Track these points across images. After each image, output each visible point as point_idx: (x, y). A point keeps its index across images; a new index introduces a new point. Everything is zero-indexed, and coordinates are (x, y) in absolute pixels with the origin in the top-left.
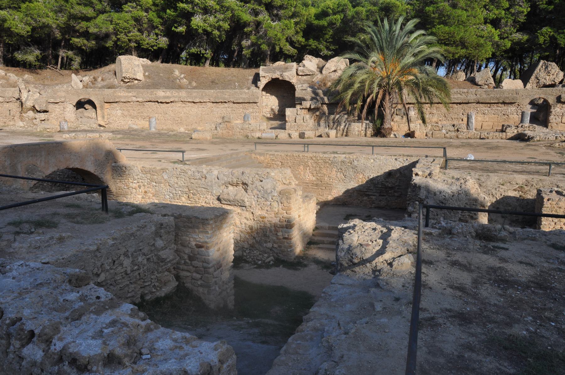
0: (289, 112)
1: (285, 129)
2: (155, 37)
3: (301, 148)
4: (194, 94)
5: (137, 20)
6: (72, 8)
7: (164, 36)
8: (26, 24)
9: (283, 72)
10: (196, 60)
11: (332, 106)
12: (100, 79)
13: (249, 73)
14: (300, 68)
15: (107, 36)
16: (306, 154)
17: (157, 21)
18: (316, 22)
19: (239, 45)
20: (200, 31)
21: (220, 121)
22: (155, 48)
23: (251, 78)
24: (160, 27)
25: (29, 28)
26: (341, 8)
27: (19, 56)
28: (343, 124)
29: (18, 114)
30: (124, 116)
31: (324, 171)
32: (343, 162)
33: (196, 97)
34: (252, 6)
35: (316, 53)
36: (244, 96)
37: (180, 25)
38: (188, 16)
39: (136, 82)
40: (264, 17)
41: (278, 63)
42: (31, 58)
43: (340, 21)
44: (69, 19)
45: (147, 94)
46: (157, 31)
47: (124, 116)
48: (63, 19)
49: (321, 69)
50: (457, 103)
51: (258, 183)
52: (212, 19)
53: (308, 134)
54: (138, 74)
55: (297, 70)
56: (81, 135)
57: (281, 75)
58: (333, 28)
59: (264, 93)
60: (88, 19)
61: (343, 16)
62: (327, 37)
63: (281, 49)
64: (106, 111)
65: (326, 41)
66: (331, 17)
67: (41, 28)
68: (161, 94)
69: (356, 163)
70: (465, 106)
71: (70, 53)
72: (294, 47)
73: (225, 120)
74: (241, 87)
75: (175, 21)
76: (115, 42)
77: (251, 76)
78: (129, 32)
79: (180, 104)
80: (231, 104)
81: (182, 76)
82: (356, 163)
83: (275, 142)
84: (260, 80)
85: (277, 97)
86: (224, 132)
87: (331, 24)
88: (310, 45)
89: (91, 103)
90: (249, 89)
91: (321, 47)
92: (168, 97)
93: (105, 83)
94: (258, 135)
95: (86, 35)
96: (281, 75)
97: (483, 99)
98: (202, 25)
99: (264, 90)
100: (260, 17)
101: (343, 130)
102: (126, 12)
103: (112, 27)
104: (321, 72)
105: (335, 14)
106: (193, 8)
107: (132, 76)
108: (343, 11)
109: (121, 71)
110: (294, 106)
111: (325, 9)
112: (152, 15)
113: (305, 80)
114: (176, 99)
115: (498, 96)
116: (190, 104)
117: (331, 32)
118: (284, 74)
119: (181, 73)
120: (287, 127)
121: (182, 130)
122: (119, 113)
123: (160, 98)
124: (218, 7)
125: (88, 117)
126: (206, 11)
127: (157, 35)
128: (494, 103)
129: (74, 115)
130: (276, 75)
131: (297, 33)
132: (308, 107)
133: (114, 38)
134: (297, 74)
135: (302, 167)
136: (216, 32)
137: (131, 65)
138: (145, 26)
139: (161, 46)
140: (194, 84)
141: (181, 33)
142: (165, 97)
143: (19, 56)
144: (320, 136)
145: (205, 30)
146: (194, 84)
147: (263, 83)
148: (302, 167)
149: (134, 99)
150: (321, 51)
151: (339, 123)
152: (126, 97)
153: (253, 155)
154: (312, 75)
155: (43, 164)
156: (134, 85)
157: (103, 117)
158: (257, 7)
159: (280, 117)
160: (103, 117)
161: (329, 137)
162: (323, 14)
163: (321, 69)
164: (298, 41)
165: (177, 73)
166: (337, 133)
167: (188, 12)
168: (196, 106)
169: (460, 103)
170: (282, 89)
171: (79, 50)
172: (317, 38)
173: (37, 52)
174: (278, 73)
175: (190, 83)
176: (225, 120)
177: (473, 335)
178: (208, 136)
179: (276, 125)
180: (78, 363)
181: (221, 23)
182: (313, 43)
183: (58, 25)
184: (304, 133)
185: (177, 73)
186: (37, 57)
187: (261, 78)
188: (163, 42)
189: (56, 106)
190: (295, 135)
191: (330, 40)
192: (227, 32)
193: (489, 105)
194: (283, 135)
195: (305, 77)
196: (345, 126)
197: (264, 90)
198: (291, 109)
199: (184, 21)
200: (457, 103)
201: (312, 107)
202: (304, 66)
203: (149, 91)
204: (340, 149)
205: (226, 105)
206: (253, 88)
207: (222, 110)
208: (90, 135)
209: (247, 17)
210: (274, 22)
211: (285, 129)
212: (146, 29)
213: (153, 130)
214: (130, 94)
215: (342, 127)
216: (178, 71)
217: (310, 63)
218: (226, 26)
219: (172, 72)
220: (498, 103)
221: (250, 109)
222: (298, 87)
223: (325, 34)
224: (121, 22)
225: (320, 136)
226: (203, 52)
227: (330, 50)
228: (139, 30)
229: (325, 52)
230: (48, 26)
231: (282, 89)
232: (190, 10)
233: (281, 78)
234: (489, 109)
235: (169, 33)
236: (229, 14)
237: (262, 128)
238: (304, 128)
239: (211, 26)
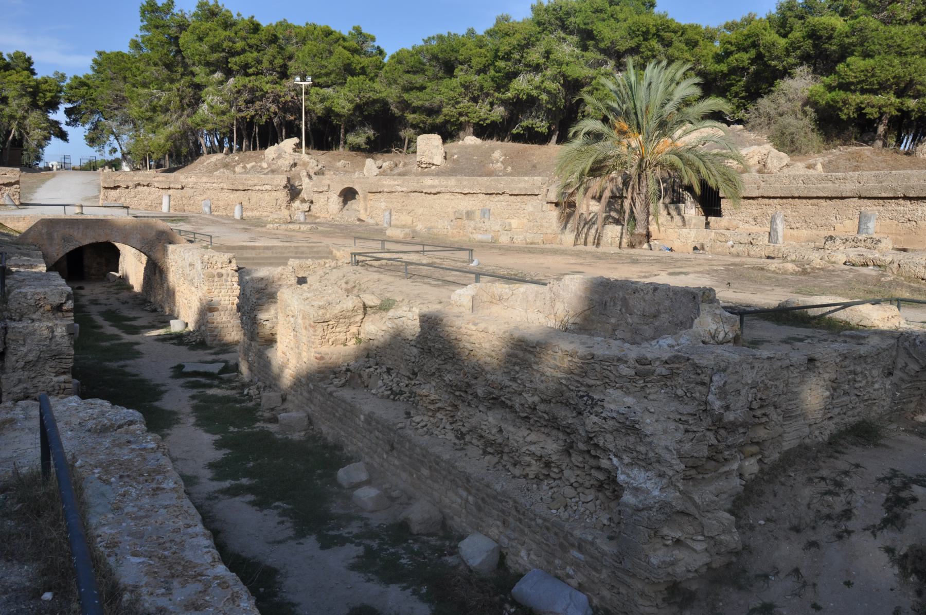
4: (465, 183)
5: (466, 86)
29: (284, 204)
33: (464, 187)
50: (826, 198)
54: (436, 158)
67: (366, 104)
70: (838, 201)
78: (458, 103)
79: (448, 196)
80: (507, 196)
92: (433, 187)
97: (867, 190)
114: (443, 189)
115: (894, 185)
116: (460, 196)
128: (891, 198)
139: (493, 119)
149: (399, 189)
155: (80, 235)
157: (366, 210)
169: (831, 198)
173: (371, 133)
177: (233, 388)
180: (415, 529)
186: (368, 138)
189: (321, 195)
191: (744, 94)
193: (881, 202)
200: (826, 198)
205: (501, 197)
214: (396, 183)
220: (897, 198)
230: (385, 103)
234: (881, 208)
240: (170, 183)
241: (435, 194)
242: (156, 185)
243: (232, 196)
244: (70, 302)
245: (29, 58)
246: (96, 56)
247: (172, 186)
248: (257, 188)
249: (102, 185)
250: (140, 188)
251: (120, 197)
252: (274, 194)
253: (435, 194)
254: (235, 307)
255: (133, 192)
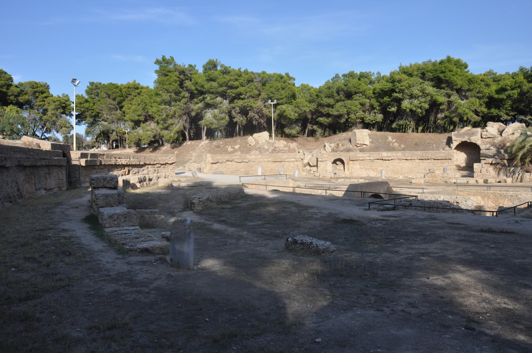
0: (476, 166)
1: (473, 177)
2: (374, 115)
3: (485, 188)
5: (362, 105)
6: (322, 100)
7: (380, 113)
8: (295, 112)
9: (470, 136)
10: (402, 129)
11: (511, 160)
12: (340, 145)
13: (443, 137)
14: (483, 133)
15: (340, 116)
16: (489, 192)
17: (376, 104)
18: (496, 96)
19: (436, 118)
20: (408, 110)
21: (428, 171)
22: (374, 122)
23: (445, 141)
24: (378, 108)
25: (297, 115)
26: (518, 85)
27: (287, 131)
28: (517, 174)
30: (361, 168)
31: (500, 201)
32: (511, 196)
33: (408, 156)
34: (446, 91)
35: (496, 119)
36: (442, 155)
37: (393, 106)
38: (399, 101)
39: (365, 146)
40: (455, 97)
41: (466, 128)
42: (294, 132)
43: (517, 94)
44: (318, 107)
45: (375, 155)
46: (375, 111)
47: (361, 168)
48: (313, 106)
49: (501, 133)
51: (464, 202)
52: (416, 102)
53: (490, 180)
55: (481, 134)
56: (348, 180)
57: (469, 139)
58: (511, 99)
59: (455, 151)
60: (331, 106)
61: (519, 90)
62: (506, 106)
63: (467, 118)
64: (350, 166)
65: (506, 109)
66: (509, 92)
68: (385, 154)
69: (520, 196)
71: (315, 127)
72: (478, 115)
73: (431, 172)
74: (438, 148)
75: (389, 104)
76: (347, 120)
77: (444, 139)
78: (357, 113)
79: (397, 161)
80: (433, 160)
81: (394, 141)
82: (520, 196)
83: (467, 185)
84: (452, 143)
85: (466, 153)
86: (430, 179)
87: (509, 96)
88: (492, 113)
89: (342, 162)
90: (444, 149)
91: (501, 113)
92: (390, 157)
93: (344, 148)
94: (454, 181)
95: (328, 115)
96: (469, 139)
98: (409, 106)
99: (455, 149)
100: (452, 98)
101: (517, 178)
102: (356, 100)
103: (346, 110)
104: (501, 135)
105: (513, 89)
106: (403, 96)
107: (362, 143)
108: (519, 87)
109: (356, 139)
110: (479, 161)
111: (504, 86)
112: (374, 101)
113: (488, 142)
114: (395, 158)
116: (404, 161)
117: (510, 102)
118: (471, 138)
119: (393, 139)
120: (475, 176)
121: (401, 178)
122: (358, 166)
123: (384, 157)
124: (421, 94)
125: (339, 170)
126: (412, 97)
127: (375, 113)
129: (331, 168)
130: (466, 139)
131: (481, 105)
132: (490, 162)
133: (346, 117)
134: (482, 137)
135: (486, 199)
136: (419, 110)
137: (363, 135)
138: (367, 108)
139: (378, 120)
140: (403, 146)
141: (393, 112)
142: (387, 157)
143: (287, 131)
144: (500, 182)
145: (411, 110)
146: (403, 146)
147: (455, 144)
148: (486, 199)
149: (368, 158)
150: (501, 116)
151: (514, 172)
152: (362, 157)
153: (456, 192)
154: (494, 138)
156: (364, 148)
157: (349, 169)
158: (450, 92)
159: (469, 168)
160: (349, 169)
161: (506, 182)
162: (502, 90)
163: (501, 133)
164: (482, 111)
165: (390, 139)
166: (513, 179)
167: (400, 98)
168: (408, 162)
170: (471, 149)
171: (321, 125)
172: (498, 107)
174: (467, 137)
175: (400, 146)
176: (431, 172)
178: (422, 181)
179: (466, 174)
181: (423, 104)
182: (494, 111)
183: (310, 110)
184: (487, 180)
185: (390, 139)
187: (453, 142)
188: (380, 117)
190: (481, 182)
192: (427, 111)
194: (472, 181)
195: (488, 140)
196: (519, 175)
197: (455, 149)
198: (478, 164)
199: (395, 104)
201: (493, 162)
202: (487, 131)
203: (377, 153)
204: (512, 189)
206: (447, 148)
207: (426, 165)
208: (352, 180)
209: (441, 99)
210: (463, 100)
211: (473, 177)
212: (368, 110)
213: (383, 177)
214: (366, 155)
215: (517, 176)
216: (390, 136)
217: (493, 128)
218: (427, 106)
219: (387, 138)
221: (446, 164)
222: (482, 147)
223: (505, 104)
224: (352, 107)
225: (500, 182)
226: (408, 123)
227: (509, 115)
228: (363, 111)
229: (505, 117)
231: (471, 149)
232: (401, 97)
233: (468, 141)
235: (384, 110)
236: (429, 98)
237: (456, 176)
238: (488, 177)
239: (415, 107)
240: (243, 159)
241: (170, 164)
242: (236, 160)
243: (273, 165)
244: (170, 233)
245: (48, 86)
246: (88, 84)
247: (244, 161)
248: (288, 160)
249: (211, 162)
250: (228, 163)
251: (218, 168)
252: (296, 163)
253: (170, 164)
254: (501, 205)
255: (224, 165)
